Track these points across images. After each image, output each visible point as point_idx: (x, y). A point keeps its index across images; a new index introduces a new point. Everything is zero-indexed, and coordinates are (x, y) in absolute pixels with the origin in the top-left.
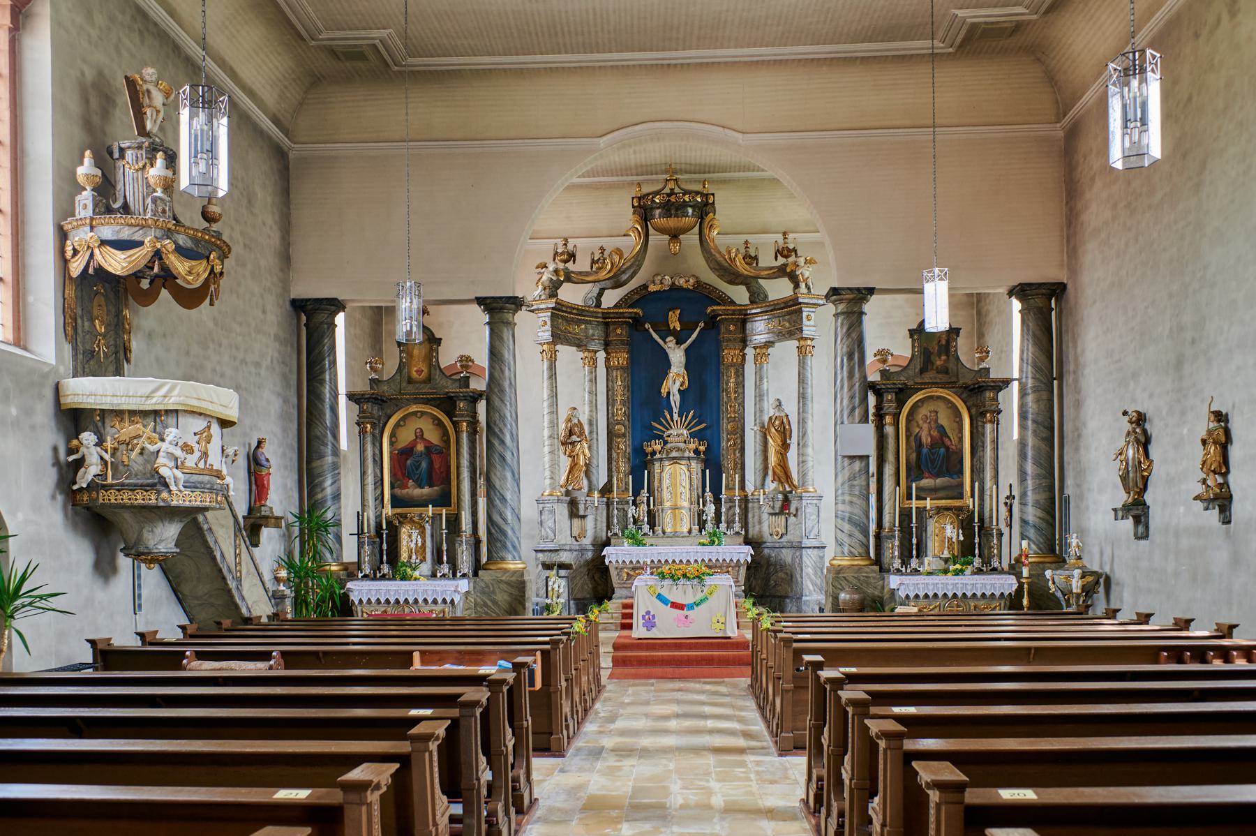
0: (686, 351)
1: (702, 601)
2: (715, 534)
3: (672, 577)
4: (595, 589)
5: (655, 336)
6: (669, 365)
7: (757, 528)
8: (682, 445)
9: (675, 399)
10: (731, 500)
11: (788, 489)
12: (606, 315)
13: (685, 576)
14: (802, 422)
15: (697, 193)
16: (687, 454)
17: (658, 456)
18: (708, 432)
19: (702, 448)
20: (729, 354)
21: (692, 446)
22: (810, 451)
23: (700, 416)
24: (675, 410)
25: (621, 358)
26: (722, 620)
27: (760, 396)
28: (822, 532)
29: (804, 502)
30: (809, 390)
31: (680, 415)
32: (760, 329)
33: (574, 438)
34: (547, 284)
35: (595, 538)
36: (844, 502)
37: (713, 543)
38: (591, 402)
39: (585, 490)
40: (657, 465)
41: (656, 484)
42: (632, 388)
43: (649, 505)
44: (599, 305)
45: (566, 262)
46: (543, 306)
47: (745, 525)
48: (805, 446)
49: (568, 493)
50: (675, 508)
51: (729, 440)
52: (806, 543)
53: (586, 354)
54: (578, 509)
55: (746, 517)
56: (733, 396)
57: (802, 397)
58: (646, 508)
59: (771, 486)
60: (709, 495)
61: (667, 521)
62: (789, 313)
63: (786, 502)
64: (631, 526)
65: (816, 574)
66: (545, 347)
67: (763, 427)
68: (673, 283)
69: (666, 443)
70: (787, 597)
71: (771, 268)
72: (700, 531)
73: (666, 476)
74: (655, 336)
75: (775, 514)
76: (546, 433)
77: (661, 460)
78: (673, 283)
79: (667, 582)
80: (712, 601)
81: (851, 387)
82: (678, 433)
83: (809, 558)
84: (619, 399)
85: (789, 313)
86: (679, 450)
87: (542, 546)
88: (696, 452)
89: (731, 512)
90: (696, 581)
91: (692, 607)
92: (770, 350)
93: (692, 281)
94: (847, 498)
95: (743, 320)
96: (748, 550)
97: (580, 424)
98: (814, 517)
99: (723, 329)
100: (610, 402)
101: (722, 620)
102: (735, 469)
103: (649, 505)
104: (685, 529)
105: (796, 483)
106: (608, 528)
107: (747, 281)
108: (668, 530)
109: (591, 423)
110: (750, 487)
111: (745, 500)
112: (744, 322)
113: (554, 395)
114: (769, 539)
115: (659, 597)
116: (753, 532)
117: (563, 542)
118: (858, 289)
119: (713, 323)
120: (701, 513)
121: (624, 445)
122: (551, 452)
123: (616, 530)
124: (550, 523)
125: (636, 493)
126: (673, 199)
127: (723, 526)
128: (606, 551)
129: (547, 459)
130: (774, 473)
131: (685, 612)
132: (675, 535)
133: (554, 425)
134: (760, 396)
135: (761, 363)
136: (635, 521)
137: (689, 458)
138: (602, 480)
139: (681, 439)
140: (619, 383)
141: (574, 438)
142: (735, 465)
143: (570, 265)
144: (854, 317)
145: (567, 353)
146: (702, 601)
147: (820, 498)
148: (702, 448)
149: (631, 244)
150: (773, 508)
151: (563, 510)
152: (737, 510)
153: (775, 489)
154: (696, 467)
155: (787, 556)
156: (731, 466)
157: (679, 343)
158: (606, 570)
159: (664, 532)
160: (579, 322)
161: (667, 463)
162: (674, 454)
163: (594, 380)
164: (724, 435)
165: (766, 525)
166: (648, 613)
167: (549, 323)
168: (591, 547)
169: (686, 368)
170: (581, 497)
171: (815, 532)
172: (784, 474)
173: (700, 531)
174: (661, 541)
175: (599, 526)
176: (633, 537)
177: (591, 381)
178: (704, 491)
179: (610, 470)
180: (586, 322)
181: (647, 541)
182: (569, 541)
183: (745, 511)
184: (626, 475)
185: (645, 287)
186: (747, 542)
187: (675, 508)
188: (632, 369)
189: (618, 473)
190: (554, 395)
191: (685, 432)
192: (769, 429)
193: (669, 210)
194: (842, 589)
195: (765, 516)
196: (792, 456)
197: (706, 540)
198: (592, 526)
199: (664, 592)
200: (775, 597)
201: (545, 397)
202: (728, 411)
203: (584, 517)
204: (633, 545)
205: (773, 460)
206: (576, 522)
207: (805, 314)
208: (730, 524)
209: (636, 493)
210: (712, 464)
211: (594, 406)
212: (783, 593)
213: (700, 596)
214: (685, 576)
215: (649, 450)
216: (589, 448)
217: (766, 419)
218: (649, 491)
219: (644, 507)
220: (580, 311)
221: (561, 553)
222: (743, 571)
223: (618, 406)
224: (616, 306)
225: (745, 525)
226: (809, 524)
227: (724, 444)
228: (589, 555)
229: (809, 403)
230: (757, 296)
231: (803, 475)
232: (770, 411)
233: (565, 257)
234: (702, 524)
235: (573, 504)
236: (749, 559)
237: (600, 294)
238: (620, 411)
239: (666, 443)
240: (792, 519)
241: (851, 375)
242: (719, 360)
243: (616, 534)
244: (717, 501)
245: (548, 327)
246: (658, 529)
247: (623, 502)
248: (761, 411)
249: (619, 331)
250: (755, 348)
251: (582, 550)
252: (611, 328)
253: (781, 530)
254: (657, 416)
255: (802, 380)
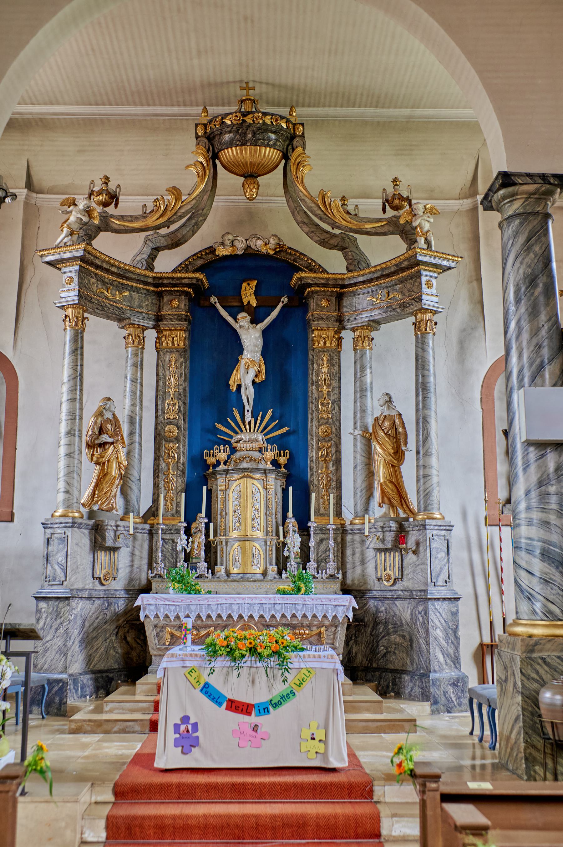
0: (264, 332)
1: (284, 698)
2: (301, 578)
3: (231, 652)
4: (127, 656)
5: (224, 313)
6: (240, 350)
7: (358, 570)
8: (256, 455)
9: (248, 393)
10: (323, 530)
11: (402, 515)
12: (158, 282)
13: (253, 650)
14: (423, 422)
15: (282, 118)
16: (262, 466)
17: (222, 467)
18: (292, 438)
19: (283, 460)
20: (320, 336)
21: (270, 455)
22: (434, 461)
23: (280, 418)
24: (248, 407)
25: (178, 337)
26: (320, 735)
27: (361, 391)
28: (454, 578)
29: (429, 534)
30: (432, 379)
31: (254, 415)
32: (364, 304)
33: (105, 438)
34: (75, 227)
35: (131, 580)
36: (530, 523)
37: (298, 590)
38: (133, 393)
39: (121, 512)
40: (221, 479)
41: (219, 506)
42: (193, 376)
43: (207, 535)
44: (150, 267)
45: (106, 204)
46: (68, 255)
47: (342, 565)
48: (427, 454)
49: (91, 515)
50: (244, 539)
51: (319, 448)
52: (434, 592)
53: (130, 331)
54: (104, 538)
55: (343, 553)
56: (325, 390)
57: (422, 388)
58: (203, 539)
59: (378, 511)
60: (292, 522)
61: (232, 558)
62: (402, 281)
63: (401, 534)
64: (182, 564)
65: (447, 639)
66: (69, 312)
67: (366, 430)
68: (248, 247)
69: (234, 450)
70: (404, 672)
71: (378, 220)
72: (280, 573)
73: (232, 494)
74: (224, 313)
75: (385, 550)
76: (63, 428)
77: (227, 472)
78: (248, 247)
79: (221, 663)
80: (303, 696)
81: (535, 332)
82: (251, 439)
83: (438, 614)
84: (172, 390)
85: (402, 281)
86: (251, 459)
87: (48, 591)
88: (275, 462)
89: (322, 547)
90: (273, 662)
91: (266, 710)
92: (374, 334)
93: (273, 241)
94: (536, 515)
95: (340, 292)
96: (349, 601)
97: (115, 421)
98: (443, 555)
99: (312, 304)
100: (160, 394)
101: (320, 735)
102: (327, 488)
103: (207, 535)
104: (258, 570)
105: (414, 505)
106: (150, 566)
107: (342, 244)
108: (235, 570)
109: (132, 421)
110: (348, 515)
111: (342, 531)
112: (340, 297)
113: (78, 376)
114: (377, 586)
115: (207, 689)
116: (354, 575)
117: (79, 586)
118: (544, 177)
119: (299, 300)
120: (281, 547)
121: (178, 452)
122: (69, 455)
123: (160, 569)
124: (60, 558)
125: (190, 519)
126: (249, 120)
127: (312, 566)
128: (142, 600)
129: (62, 464)
130: (383, 492)
131: (253, 719)
132: (244, 578)
133: (75, 417)
134: (361, 391)
135: (363, 349)
136: (188, 557)
137: (265, 471)
138: (145, 504)
139: (255, 446)
140: (173, 370)
141: (105, 438)
142: (329, 481)
143: (111, 210)
144: (535, 222)
145: (102, 333)
146: (284, 698)
147: (450, 528)
148: (283, 460)
149: (190, 182)
150: (383, 541)
151: (81, 540)
152: (332, 544)
153: (385, 516)
154: (275, 484)
155: (404, 610)
156: (322, 484)
157: (255, 321)
158: (140, 628)
159: (228, 574)
160: (123, 287)
161: (235, 476)
162: (244, 465)
163: (139, 365)
164: (313, 442)
165: (373, 565)
166: (185, 719)
167: (76, 280)
168: (123, 594)
169: (263, 354)
170: (110, 522)
171: (444, 576)
172: (396, 495)
173: (280, 573)
174: (222, 586)
175: (137, 563)
176: (181, 580)
177: (135, 365)
178: (285, 517)
179: (156, 486)
180: (132, 289)
181: (203, 585)
182: (89, 583)
183: (342, 546)
184: (178, 494)
185: (211, 250)
186: (346, 591)
187: (244, 539)
188: (194, 350)
189: (168, 490)
190: (78, 376)
191: (260, 437)
192: (375, 432)
193: (244, 134)
194: (543, 684)
195: (370, 553)
196: (408, 470)
197: (287, 586)
198: (126, 563)
199: (216, 682)
200: (386, 670)
201: (65, 378)
202: (318, 410)
203: (114, 549)
204: (181, 591)
205: (381, 474)
206: (102, 557)
207: (424, 279)
208: (321, 563)
209: (190, 519)
210: (297, 493)
211: (137, 398)
212: (398, 666)
213: (280, 688)
214: (253, 650)
215: (211, 460)
216: (129, 454)
217: (370, 421)
218: (209, 515)
219: (200, 539)
220: (123, 273)
221: (74, 603)
222: (341, 633)
223: (170, 400)
224: (175, 271)
225: (342, 565)
226: (437, 565)
227: (312, 454)
228: (120, 605)
229: (432, 396)
230: (355, 261)
231: (425, 495)
232: (375, 408)
233: (103, 197)
234: (282, 564)
235: (97, 531)
236: (351, 615)
237: (152, 257)
238: (173, 408)
239: (234, 450)
240: (410, 558)
241: (533, 313)
242: (304, 345)
243: (160, 576)
244: (304, 530)
245: (75, 286)
246: (220, 569)
247: (172, 530)
248: (364, 411)
249: (175, 303)
250: (353, 330)
251: (109, 598)
252: (166, 299)
253: (394, 573)
254: (223, 415)
255: (421, 365)
